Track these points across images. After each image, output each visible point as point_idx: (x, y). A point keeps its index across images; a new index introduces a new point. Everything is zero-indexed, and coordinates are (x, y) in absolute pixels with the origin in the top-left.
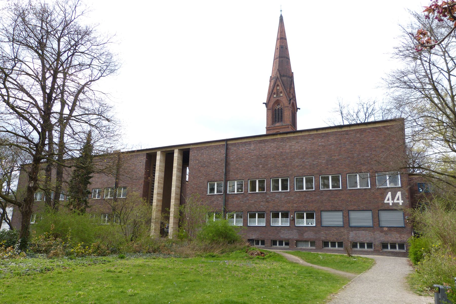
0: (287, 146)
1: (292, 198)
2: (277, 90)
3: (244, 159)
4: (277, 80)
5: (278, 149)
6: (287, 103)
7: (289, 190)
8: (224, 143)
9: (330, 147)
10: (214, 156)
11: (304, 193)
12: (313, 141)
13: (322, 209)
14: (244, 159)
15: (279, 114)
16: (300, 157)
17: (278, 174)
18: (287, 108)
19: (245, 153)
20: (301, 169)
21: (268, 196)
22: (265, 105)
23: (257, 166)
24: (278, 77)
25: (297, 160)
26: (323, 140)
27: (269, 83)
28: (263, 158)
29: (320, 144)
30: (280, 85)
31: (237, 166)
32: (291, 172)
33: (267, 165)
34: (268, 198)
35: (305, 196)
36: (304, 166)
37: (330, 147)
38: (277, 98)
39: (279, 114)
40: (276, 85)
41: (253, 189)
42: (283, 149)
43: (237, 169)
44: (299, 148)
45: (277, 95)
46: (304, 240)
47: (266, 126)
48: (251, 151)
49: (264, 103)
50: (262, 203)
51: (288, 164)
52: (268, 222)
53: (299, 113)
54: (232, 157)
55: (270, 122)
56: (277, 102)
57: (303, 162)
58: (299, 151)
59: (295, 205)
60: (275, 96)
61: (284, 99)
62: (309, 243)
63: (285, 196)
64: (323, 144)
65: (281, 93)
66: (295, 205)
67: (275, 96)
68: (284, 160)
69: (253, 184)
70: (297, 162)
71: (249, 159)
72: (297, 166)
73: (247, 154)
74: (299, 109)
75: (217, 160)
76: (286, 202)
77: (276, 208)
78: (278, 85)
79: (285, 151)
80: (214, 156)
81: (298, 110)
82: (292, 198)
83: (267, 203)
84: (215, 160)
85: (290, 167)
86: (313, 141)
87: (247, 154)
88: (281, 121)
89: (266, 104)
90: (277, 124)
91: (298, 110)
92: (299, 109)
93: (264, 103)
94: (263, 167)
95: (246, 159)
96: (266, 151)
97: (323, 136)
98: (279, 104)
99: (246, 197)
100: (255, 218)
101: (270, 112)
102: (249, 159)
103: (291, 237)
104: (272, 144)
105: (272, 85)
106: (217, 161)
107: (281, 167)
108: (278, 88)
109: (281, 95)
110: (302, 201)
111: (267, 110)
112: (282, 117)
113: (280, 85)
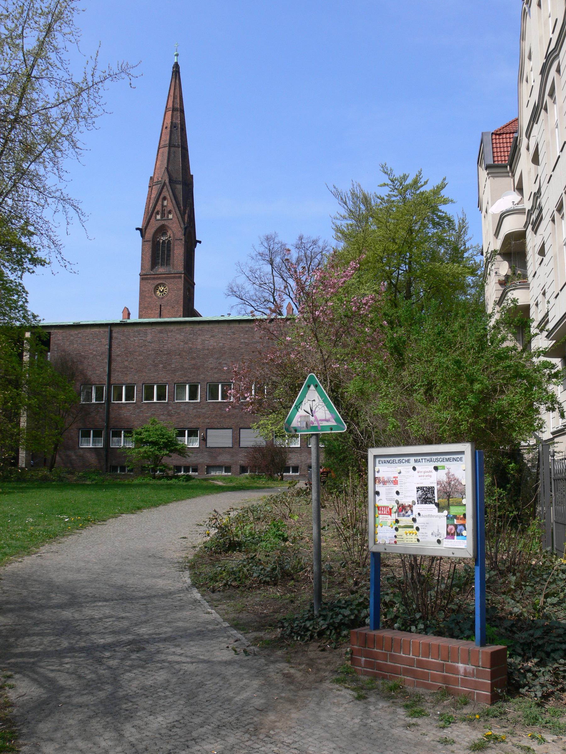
0: (199, 340)
1: (204, 411)
2: (163, 206)
3: (137, 354)
4: (163, 188)
5: (186, 343)
6: (180, 234)
7: (199, 401)
8: (107, 329)
9: (255, 346)
10: (91, 347)
11: (219, 405)
12: (234, 336)
13: (241, 426)
14: (137, 354)
15: (163, 252)
16: (216, 356)
17: (185, 379)
18: (178, 241)
19: (138, 346)
20: (216, 373)
21: (170, 408)
22: (139, 232)
23: (156, 366)
24: (165, 183)
25: (211, 360)
26: (246, 336)
27: (147, 189)
28: (164, 355)
29: (242, 340)
30: (168, 197)
31: (126, 363)
32: (202, 376)
33: (170, 365)
34: (171, 411)
35: (220, 408)
36: (220, 369)
37: (255, 346)
38: (163, 222)
39: (163, 252)
40: (162, 196)
41: (149, 396)
42: (192, 344)
43: (126, 367)
44: (215, 344)
45: (163, 215)
46: (218, 464)
47: (139, 271)
48: (147, 344)
49: (137, 229)
50: (163, 417)
51: (199, 364)
52: (107, 442)
53: (199, 251)
54: (116, 351)
55: (148, 265)
56: (162, 230)
57: (220, 363)
58: (214, 349)
59: (207, 421)
60: (159, 217)
61: (175, 225)
62: (224, 469)
63: (194, 408)
64: (246, 341)
65: (170, 212)
66: (207, 421)
67: (159, 217)
68: (194, 359)
69: (149, 389)
70: (211, 363)
71: (144, 355)
72: (212, 369)
73: (142, 347)
74: (200, 242)
75: (95, 353)
76: (195, 416)
77: (181, 424)
78: (165, 198)
79: (195, 346)
80: (91, 347)
81: (198, 244)
82: (204, 411)
83: (169, 418)
84: (92, 354)
85: (201, 369)
86: (234, 336)
87: (142, 347)
88: (168, 264)
89: (142, 231)
90: (161, 270)
91: (198, 244)
92: (200, 242)
93: (137, 229)
94: (164, 367)
95: (140, 355)
96: (169, 345)
97: (247, 331)
98: (164, 234)
99: (139, 408)
100: (185, 436)
101: (149, 245)
102: (144, 355)
103: (201, 461)
104: (178, 336)
105: (153, 196)
106: (95, 355)
107: (189, 369)
108: (165, 203)
109: (171, 216)
110: (216, 415)
111: (144, 241)
112: (169, 256)
113: (168, 197)
